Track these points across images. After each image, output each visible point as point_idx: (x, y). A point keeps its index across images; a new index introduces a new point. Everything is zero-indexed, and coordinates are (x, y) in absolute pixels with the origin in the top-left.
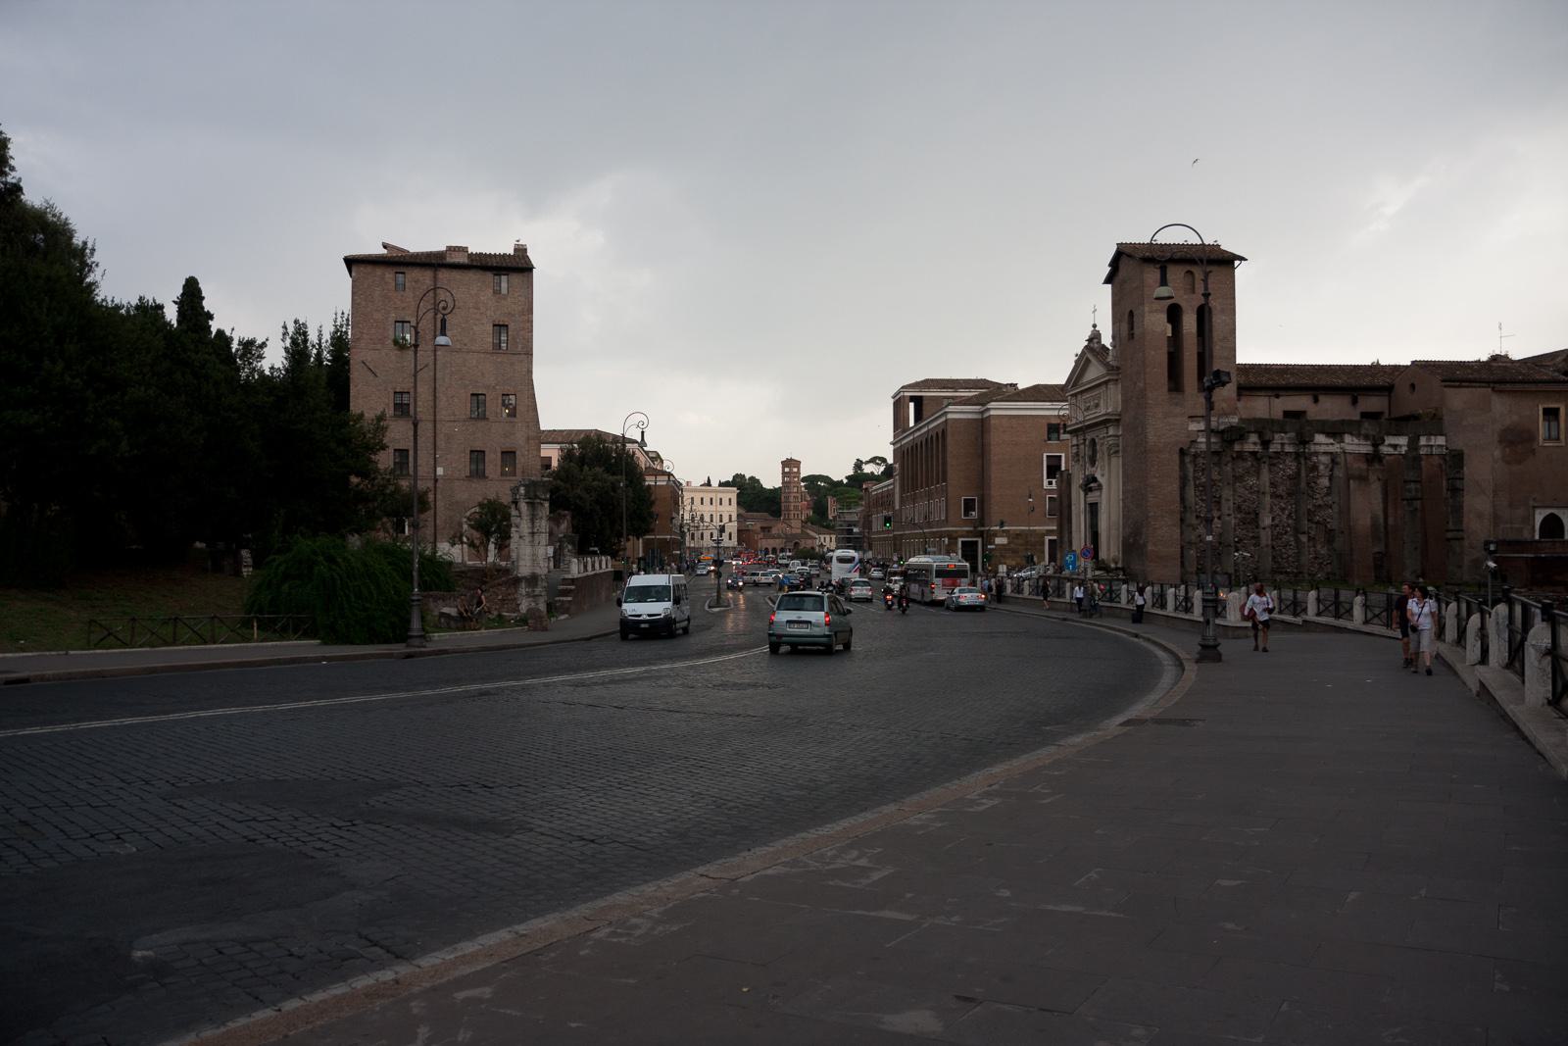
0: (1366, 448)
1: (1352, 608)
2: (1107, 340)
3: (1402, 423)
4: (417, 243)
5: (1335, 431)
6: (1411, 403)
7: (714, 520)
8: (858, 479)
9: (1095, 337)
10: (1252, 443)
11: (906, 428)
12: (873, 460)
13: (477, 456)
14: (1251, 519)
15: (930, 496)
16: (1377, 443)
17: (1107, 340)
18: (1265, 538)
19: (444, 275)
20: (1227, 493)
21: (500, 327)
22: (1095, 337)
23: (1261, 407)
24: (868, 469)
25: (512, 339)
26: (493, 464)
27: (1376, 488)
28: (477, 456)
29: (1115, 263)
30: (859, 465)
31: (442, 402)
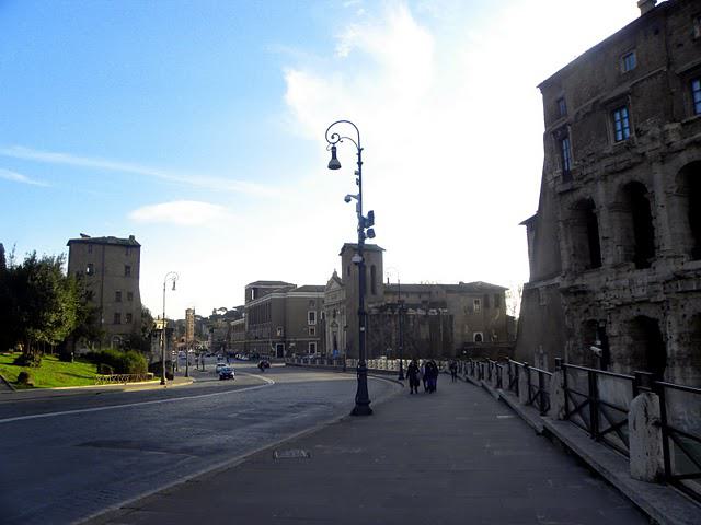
0: (424, 313)
1: (669, 220)
2: (340, 275)
3: (434, 305)
4: (94, 235)
5: (415, 307)
6: (436, 298)
7: (339, 347)
8: (215, 317)
9: (335, 273)
10: (389, 312)
11: (251, 300)
12: (221, 309)
13: (117, 315)
14: (389, 337)
15: (264, 327)
16: (427, 311)
17: (340, 275)
18: (394, 343)
19: (106, 247)
20: (381, 329)
21: (127, 267)
22: (335, 273)
23: (390, 299)
24: (218, 313)
25: (132, 271)
26: (123, 319)
27: (427, 326)
28: (117, 315)
29: (343, 249)
30: (215, 311)
31: (105, 295)
